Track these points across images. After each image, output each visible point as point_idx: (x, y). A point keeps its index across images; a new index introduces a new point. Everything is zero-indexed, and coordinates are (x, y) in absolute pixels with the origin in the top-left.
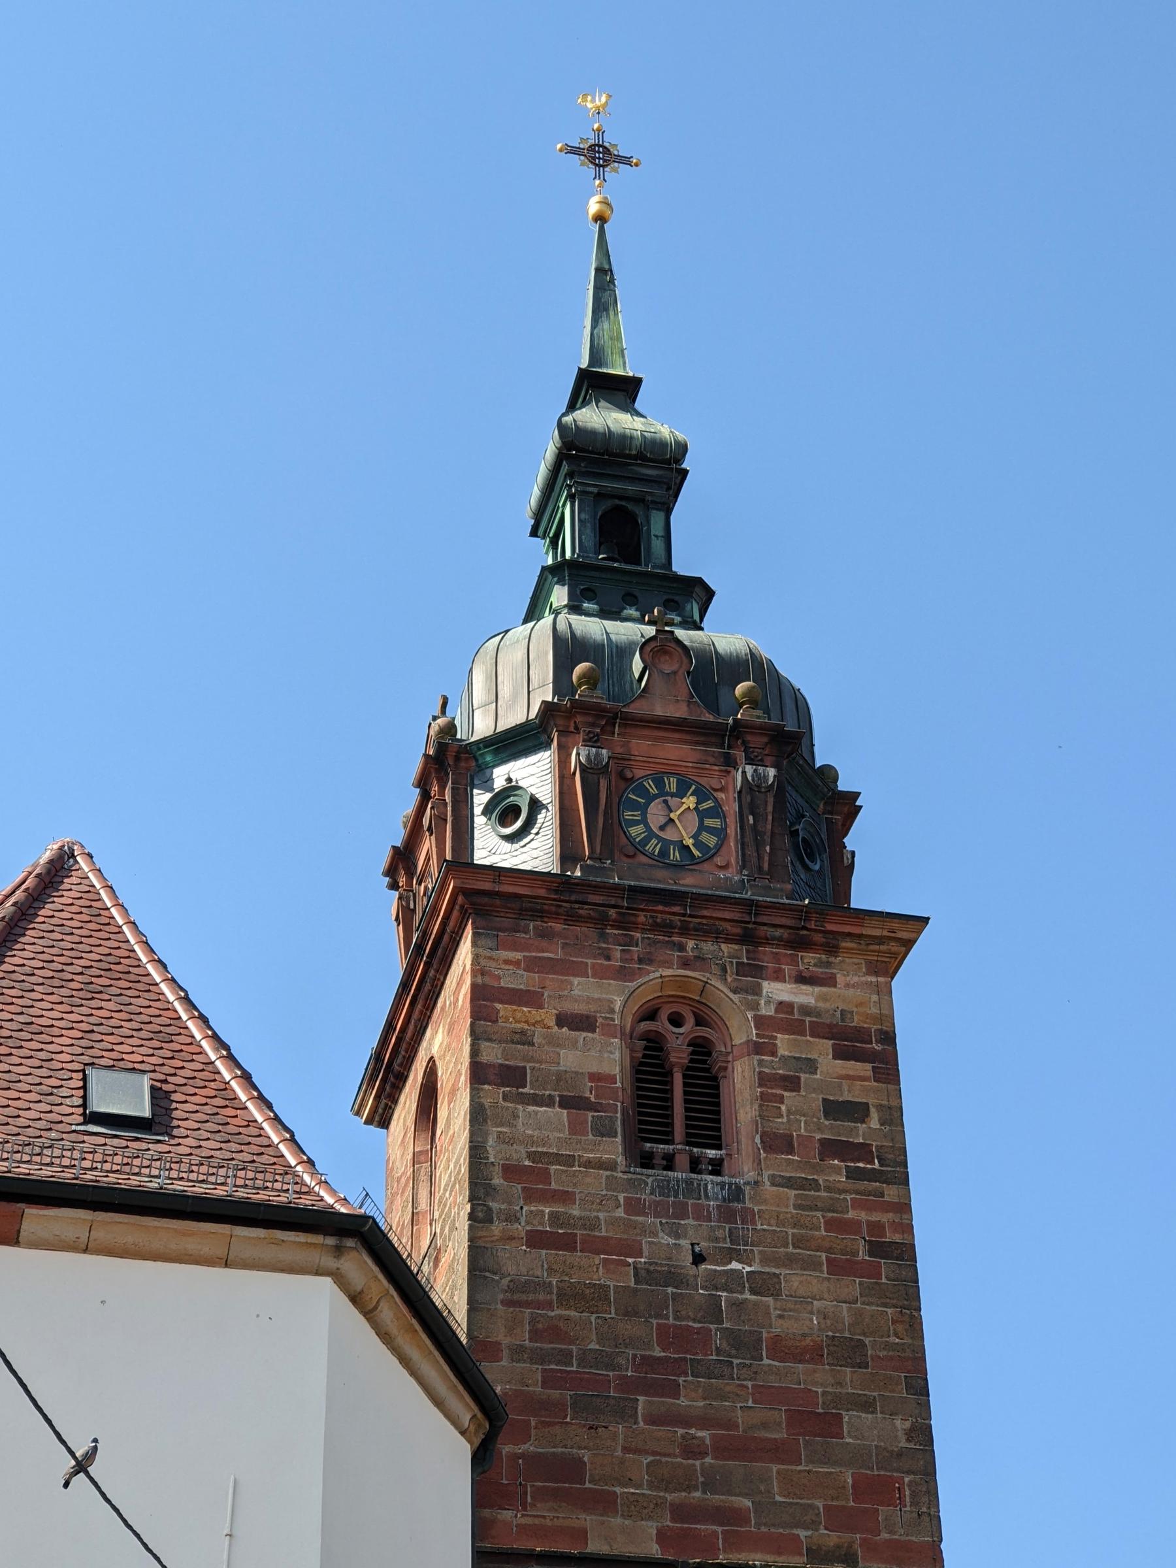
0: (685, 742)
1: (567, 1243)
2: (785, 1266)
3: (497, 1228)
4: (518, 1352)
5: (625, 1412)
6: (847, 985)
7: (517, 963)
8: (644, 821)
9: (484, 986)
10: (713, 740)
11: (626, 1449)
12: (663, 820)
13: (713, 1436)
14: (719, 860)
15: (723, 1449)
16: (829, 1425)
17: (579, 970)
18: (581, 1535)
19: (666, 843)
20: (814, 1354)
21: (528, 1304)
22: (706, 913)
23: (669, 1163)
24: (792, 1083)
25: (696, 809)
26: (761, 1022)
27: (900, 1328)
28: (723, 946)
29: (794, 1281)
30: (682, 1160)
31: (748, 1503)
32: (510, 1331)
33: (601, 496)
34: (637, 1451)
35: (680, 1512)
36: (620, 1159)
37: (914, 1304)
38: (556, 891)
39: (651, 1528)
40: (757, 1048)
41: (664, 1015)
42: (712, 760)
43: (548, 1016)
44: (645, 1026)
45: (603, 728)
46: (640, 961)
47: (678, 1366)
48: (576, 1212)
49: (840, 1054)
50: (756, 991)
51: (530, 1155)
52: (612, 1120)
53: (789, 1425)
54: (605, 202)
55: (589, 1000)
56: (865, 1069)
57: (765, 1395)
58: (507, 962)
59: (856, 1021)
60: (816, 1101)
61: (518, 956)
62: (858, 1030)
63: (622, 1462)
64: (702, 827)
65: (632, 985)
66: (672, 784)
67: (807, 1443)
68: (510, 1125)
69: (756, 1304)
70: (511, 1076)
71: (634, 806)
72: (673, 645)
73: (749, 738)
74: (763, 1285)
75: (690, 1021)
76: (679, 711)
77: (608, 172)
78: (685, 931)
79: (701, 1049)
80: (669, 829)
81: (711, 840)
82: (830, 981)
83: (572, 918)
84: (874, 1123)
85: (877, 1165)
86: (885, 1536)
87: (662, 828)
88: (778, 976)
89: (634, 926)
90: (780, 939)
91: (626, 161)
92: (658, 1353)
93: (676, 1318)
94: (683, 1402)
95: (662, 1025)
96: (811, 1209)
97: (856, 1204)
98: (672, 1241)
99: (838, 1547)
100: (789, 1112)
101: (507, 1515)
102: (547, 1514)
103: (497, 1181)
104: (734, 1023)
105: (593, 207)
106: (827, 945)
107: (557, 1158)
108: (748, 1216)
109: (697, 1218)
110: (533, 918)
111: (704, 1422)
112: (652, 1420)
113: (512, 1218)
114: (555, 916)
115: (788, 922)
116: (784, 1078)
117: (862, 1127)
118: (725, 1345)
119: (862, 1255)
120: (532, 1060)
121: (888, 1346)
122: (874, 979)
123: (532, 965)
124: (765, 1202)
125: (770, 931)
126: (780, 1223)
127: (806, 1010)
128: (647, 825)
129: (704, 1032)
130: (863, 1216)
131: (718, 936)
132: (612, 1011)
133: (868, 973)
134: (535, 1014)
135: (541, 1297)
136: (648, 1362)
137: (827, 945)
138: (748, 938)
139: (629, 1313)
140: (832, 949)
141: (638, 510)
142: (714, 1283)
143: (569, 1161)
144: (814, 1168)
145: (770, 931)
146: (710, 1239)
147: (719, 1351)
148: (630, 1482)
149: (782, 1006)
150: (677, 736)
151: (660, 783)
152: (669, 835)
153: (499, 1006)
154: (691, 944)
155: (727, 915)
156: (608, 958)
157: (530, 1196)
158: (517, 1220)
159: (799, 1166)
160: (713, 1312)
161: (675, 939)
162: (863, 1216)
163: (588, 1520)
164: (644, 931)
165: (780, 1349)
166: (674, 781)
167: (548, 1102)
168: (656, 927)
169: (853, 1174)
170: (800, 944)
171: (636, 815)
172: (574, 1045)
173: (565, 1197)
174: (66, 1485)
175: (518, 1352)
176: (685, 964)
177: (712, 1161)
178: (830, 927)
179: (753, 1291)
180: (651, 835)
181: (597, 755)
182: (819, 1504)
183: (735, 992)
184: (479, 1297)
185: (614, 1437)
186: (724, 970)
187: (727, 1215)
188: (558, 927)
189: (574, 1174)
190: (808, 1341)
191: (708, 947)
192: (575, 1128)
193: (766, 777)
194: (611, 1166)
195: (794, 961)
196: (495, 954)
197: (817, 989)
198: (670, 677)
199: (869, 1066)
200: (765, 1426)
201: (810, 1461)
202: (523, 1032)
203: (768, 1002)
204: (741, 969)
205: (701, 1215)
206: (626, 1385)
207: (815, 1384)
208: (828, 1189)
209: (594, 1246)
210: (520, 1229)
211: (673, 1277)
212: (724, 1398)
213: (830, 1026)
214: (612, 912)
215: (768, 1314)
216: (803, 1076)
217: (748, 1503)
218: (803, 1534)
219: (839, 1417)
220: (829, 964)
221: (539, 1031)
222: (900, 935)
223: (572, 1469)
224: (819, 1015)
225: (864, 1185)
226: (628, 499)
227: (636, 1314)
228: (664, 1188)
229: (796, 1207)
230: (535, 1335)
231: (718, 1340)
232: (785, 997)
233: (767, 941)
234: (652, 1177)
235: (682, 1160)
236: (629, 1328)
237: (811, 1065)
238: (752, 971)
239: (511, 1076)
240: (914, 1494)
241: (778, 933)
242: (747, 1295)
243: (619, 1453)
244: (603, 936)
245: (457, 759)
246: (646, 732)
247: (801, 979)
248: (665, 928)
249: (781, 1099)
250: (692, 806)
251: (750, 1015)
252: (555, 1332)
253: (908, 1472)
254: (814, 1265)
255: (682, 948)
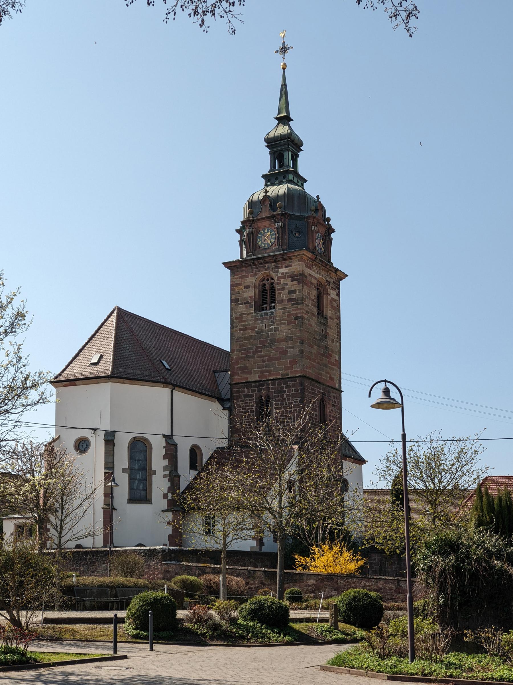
3: (234, 329)
5: (253, 357)
8: (261, 240)
11: (254, 363)
16: (286, 352)
17: (247, 276)
18: (247, 378)
20: (284, 340)
21: (239, 341)
29: (281, 327)
31: (272, 368)
32: (236, 347)
34: (256, 363)
35: (262, 372)
37: (238, 334)
39: (257, 375)
41: (265, 280)
43: (242, 287)
44: (262, 283)
46: (258, 271)
49: (292, 281)
50: (278, 272)
51: (240, 315)
58: (236, 278)
59: (295, 273)
60: (287, 291)
61: (238, 276)
63: (253, 365)
65: (256, 277)
74: (276, 329)
78: (265, 263)
82: (291, 266)
87: (264, 241)
88: (282, 267)
92: (259, 345)
95: (265, 282)
102: (242, 376)
103: (235, 321)
107: (244, 314)
108: (274, 317)
112: (258, 357)
113: (237, 327)
114: (243, 267)
116: (282, 288)
117: (295, 294)
121: (296, 336)
127: (286, 273)
131: (271, 262)
136: (258, 348)
139: (255, 339)
142: (268, 331)
143: (245, 314)
145: (279, 259)
147: (269, 343)
148: (254, 368)
149: (283, 273)
154: (267, 265)
157: (240, 322)
160: (268, 336)
162: (294, 312)
163: (248, 376)
165: (279, 341)
167: (242, 304)
170: (285, 260)
173: (245, 321)
174: (370, 396)
175: (238, 350)
176: (266, 270)
178: (288, 256)
181: (250, 230)
185: (252, 361)
187: (271, 318)
188: (244, 268)
191: (270, 265)
192: (247, 308)
194: (252, 313)
197: (289, 268)
199: (297, 282)
200: (275, 355)
205: (267, 319)
206: (254, 352)
207: (284, 345)
208: (288, 308)
210: (238, 328)
211: (262, 332)
215: (277, 334)
218: (281, 372)
219: (287, 351)
220: (291, 262)
221: (241, 290)
223: (245, 368)
224: (289, 273)
225: (295, 306)
227: (256, 339)
229: (283, 313)
231: (269, 341)
232: (283, 271)
233: (279, 261)
235: (268, 308)
238: (278, 267)
240: (299, 362)
242: (274, 332)
246: (260, 221)
247: (286, 267)
255: (265, 266)
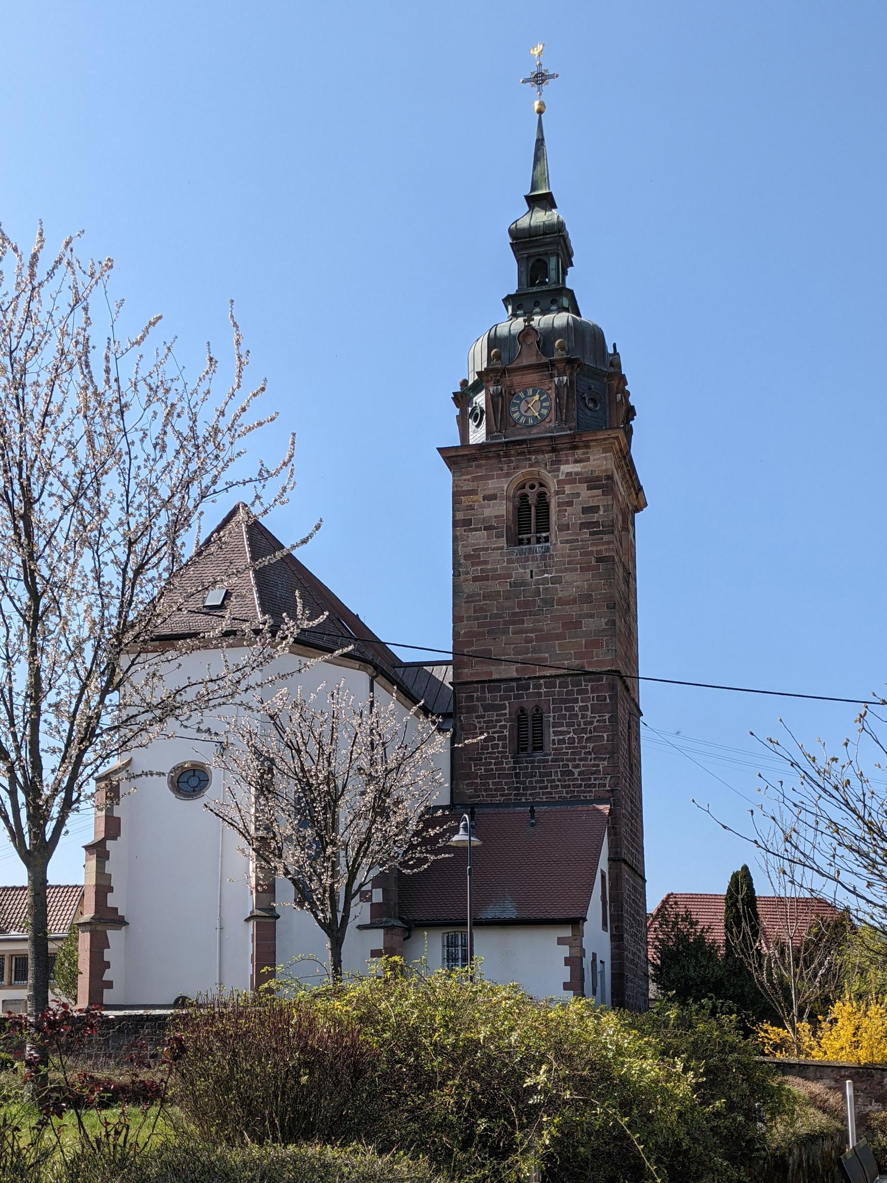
0: (533, 373)
1: (486, 578)
2: (564, 572)
3: (462, 578)
4: (469, 618)
5: (505, 632)
6: (594, 460)
7: (469, 480)
8: (519, 410)
9: (457, 491)
10: (544, 369)
12: (526, 408)
13: (536, 636)
14: (547, 420)
15: (538, 639)
16: (578, 624)
17: (491, 477)
19: (527, 417)
20: (574, 601)
21: (472, 602)
22: (535, 445)
23: (529, 541)
24: (570, 503)
25: (539, 400)
26: (559, 482)
27: (606, 587)
28: (546, 455)
29: (567, 577)
30: (533, 540)
31: (547, 655)
33: (529, 257)
34: (510, 644)
36: (505, 545)
38: (479, 450)
40: (557, 493)
41: (527, 486)
42: (545, 378)
43: (480, 497)
45: (500, 376)
46: (514, 469)
47: (524, 614)
48: (489, 567)
50: (558, 470)
52: (503, 532)
53: (562, 627)
54: (542, 104)
55: (495, 488)
56: (599, 492)
57: (553, 619)
58: (465, 480)
61: (469, 477)
62: (597, 477)
63: (504, 648)
64: (542, 407)
65: (511, 479)
66: (530, 392)
67: (569, 632)
68: (466, 540)
69: (552, 587)
70: (467, 523)
71: (515, 405)
72: (531, 331)
73: (557, 365)
75: (537, 486)
76: (533, 361)
77: (544, 87)
78: (530, 453)
79: (542, 496)
80: (528, 412)
81: (545, 412)
82: (588, 460)
83: (488, 458)
84: (601, 512)
85: (601, 528)
86: (595, 659)
87: (526, 412)
88: (567, 462)
89: (511, 456)
90: (566, 448)
91: (552, 76)
92: (517, 610)
93: (524, 597)
94: (525, 625)
95: (527, 490)
96: (574, 550)
97: (592, 545)
98: (523, 571)
99: (578, 665)
100: (569, 515)
101: (466, 670)
103: (462, 561)
104: (551, 484)
105: (536, 107)
106: (585, 446)
109: (532, 561)
110: (474, 461)
111: (532, 631)
113: (467, 573)
114: (481, 459)
115: (568, 441)
116: (567, 502)
117: (596, 515)
118: (541, 604)
119: (594, 563)
120: (474, 515)
122: (604, 455)
123: (474, 479)
124: (558, 550)
125: (562, 446)
126: (563, 557)
127: (577, 474)
128: (520, 412)
129: (543, 489)
130: (594, 548)
131: (543, 452)
132: (503, 490)
133: (603, 453)
134: (475, 497)
135: (477, 598)
136: (514, 614)
137: (585, 446)
138: (554, 450)
140: (588, 447)
141: (544, 258)
142: (538, 583)
143: (487, 549)
144: (578, 534)
145: (562, 446)
146: (537, 568)
149: (569, 474)
150: (530, 371)
151: (525, 393)
152: (529, 414)
153: (462, 498)
154: (534, 457)
155: (544, 444)
156: (502, 470)
158: (469, 573)
159: (571, 535)
160: (537, 593)
161: (527, 457)
162: (594, 548)
163: (493, 668)
164: (515, 456)
165: (562, 602)
166: (531, 390)
167: (480, 529)
168: (519, 454)
169: (591, 534)
171: (516, 409)
172: (489, 506)
173: (486, 562)
175: (469, 618)
176: (531, 466)
177: (545, 538)
179: (552, 583)
180: (522, 415)
182: (572, 652)
183: (550, 473)
184: (456, 602)
186: (546, 465)
187: (543, 558)
188: (483, 462)
189: (489, 553)
190: (571, 597)
191: (540, 457)
193: (563, 381)
194: (502, 548)
195: (573, 454)
196: (461, 478)
198: (529, 346)
199: (601, 490)
200: (554, 629)
201: (570, 638)
202: (471, 506)
203: (562, 474)
204: (553, 463)
207: (573, 612)
208: (582, 541)
209: (494, 578)
210: (470, 576)
211: (524, 583)
212: (540, 622)
213: (586, 478)
214: (501, 453)
215: (557, 590)
216: (575, 500)
217: (547, 655)
220: (587, 453)
222: (612, 436)
224: (582, 474)
226: (541, 255)
227: (510, 598)
228: (521, 552)
230: (475, 611)
232: (569, 470)
233: (562, 450)
234: (516, 549)
235: (533, 540)
236: (507, 604)
237: (578, 495)
239: (467, 523)
241: (565, 446)
242: (550, 585)
243: (503, 645)
244: (500, 462)
245: (462, 397)
247: (576, 461)
248: (523, 453)
249: (566, 511)
250: (537, 399)
251: (555, 480)
252: (482, 609)
253: (605, 636)
254: (576, 570)
255: (530, 459)
